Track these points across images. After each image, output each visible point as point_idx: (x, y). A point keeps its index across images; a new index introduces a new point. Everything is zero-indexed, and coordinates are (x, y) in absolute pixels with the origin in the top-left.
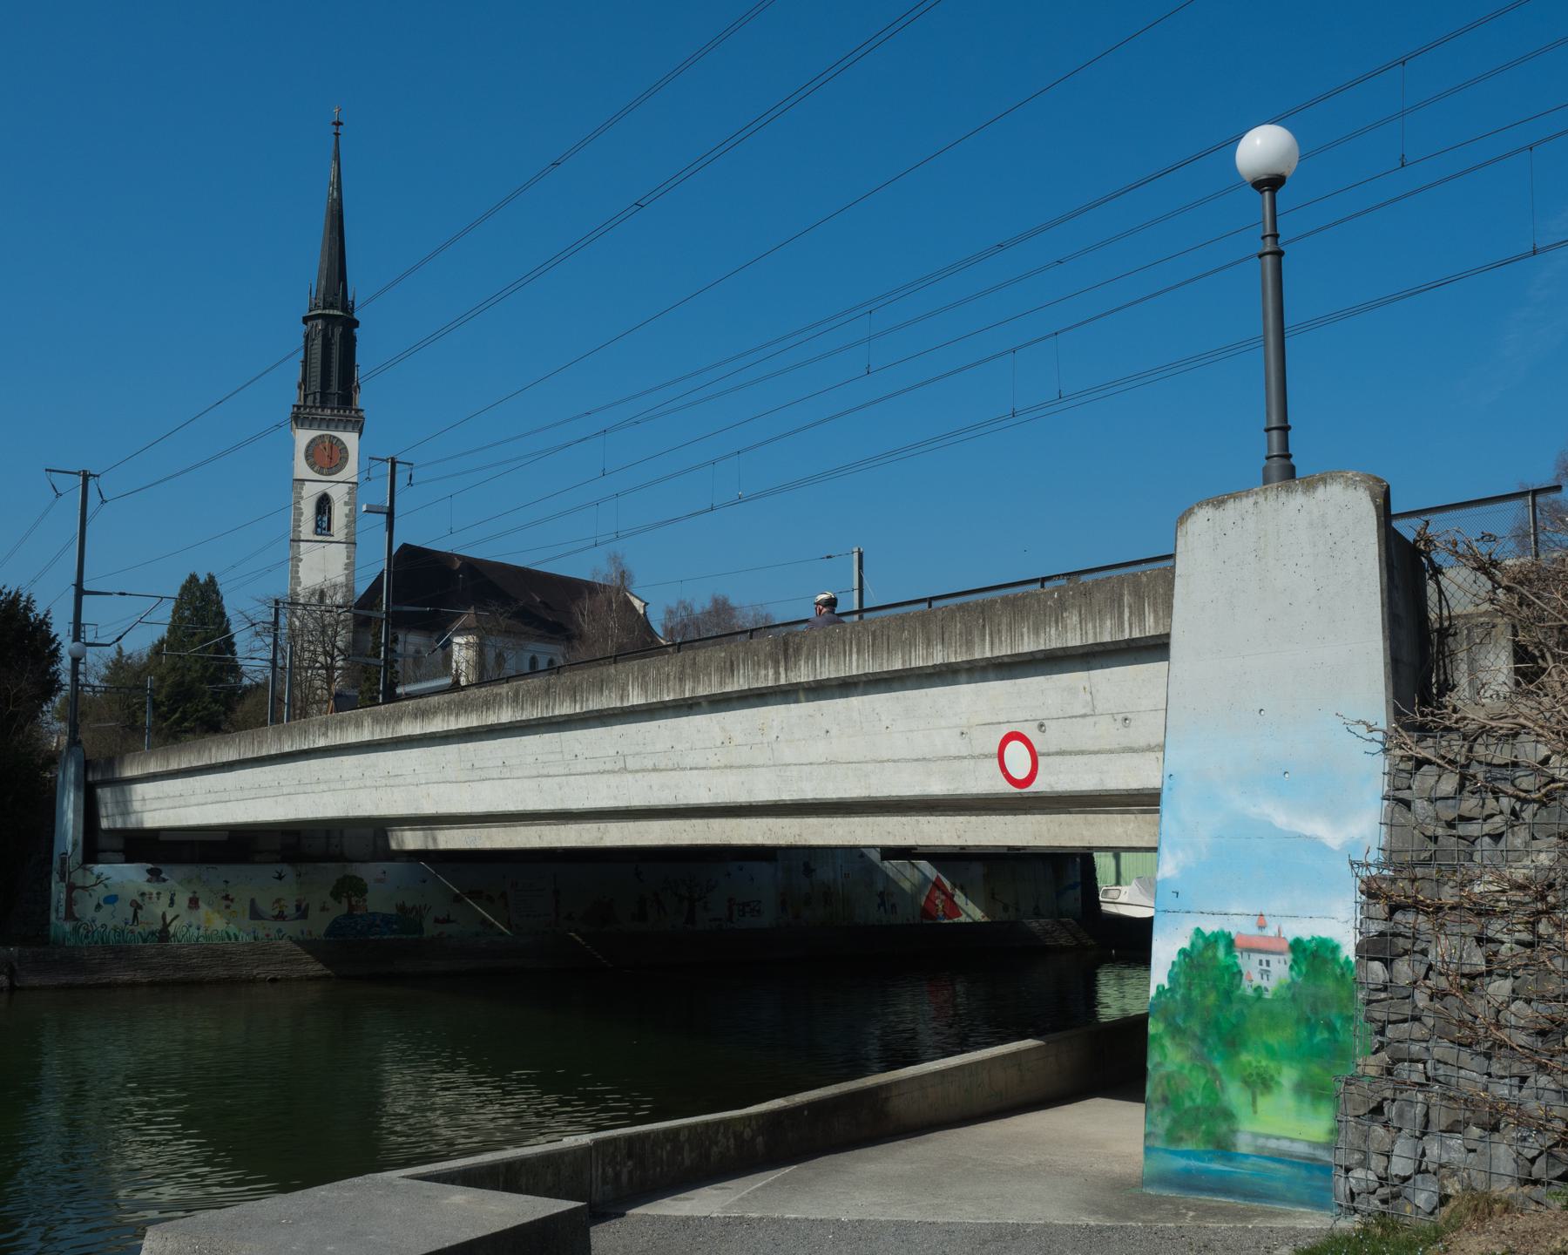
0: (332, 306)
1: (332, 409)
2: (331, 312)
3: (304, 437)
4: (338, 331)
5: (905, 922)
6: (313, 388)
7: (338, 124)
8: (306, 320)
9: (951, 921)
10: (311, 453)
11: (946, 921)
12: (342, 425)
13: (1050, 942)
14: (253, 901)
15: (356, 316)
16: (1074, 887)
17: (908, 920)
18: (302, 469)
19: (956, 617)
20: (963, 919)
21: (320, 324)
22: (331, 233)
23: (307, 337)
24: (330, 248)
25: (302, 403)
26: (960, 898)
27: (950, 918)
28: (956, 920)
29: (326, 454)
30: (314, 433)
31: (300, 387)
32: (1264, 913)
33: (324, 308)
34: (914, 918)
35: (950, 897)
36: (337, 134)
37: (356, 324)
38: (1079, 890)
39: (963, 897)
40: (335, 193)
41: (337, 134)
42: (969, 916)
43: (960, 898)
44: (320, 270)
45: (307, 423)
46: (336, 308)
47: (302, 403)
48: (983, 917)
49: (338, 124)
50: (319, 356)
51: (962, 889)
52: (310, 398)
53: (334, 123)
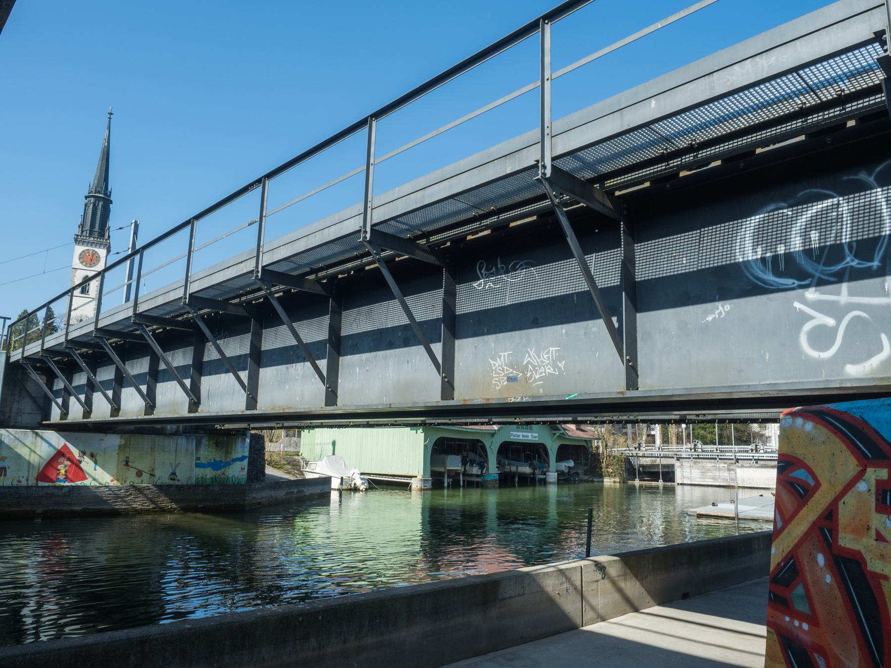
0: (99, 192)
1: (94, 238)
2: (98, 195)
3: (79, 249)
4: (101, 203)
5: (15, 483)
6: (86, 228)
7: (111, 114)
8: (86, 197)
9: (73, 484)
10: (82, 257)
11: (67, 484)
12: (98, 246)
13: (120, 506)
14: (416, 477)
15: (112, 199)
16: (242, 459)
17: (19, 481)
18: (76, 263)
19: (641, 435)
20: (88, 482)
21: (92, 200)
22: (102, 160)
23: (86, 205)
24: (101, 167)
25: (80, 234)
26: (87, 465)
27: (72, 481)
28: (79, 483)
29: (89, 258)
30: (84, 248)
31: (79, 227)
32: (149, 476)
33: (95, 193)
34: (27, 480)
35: (77, 464)
36: (110, 118)
37: (111, 202)
38: (246, 462)
39: (92, 464)
40: (106, 144)
41: (110, 118)
42: (94, 479)
43: (87, 465)
44: (96, 176)
45: (81, 243)
46: (101, 194)
47: (80, 234)
48: (112, 481)
49: (111, 114)
50: (90, 214)
51: (92, 456)
52: (85, 232)
53: (109, 113)
